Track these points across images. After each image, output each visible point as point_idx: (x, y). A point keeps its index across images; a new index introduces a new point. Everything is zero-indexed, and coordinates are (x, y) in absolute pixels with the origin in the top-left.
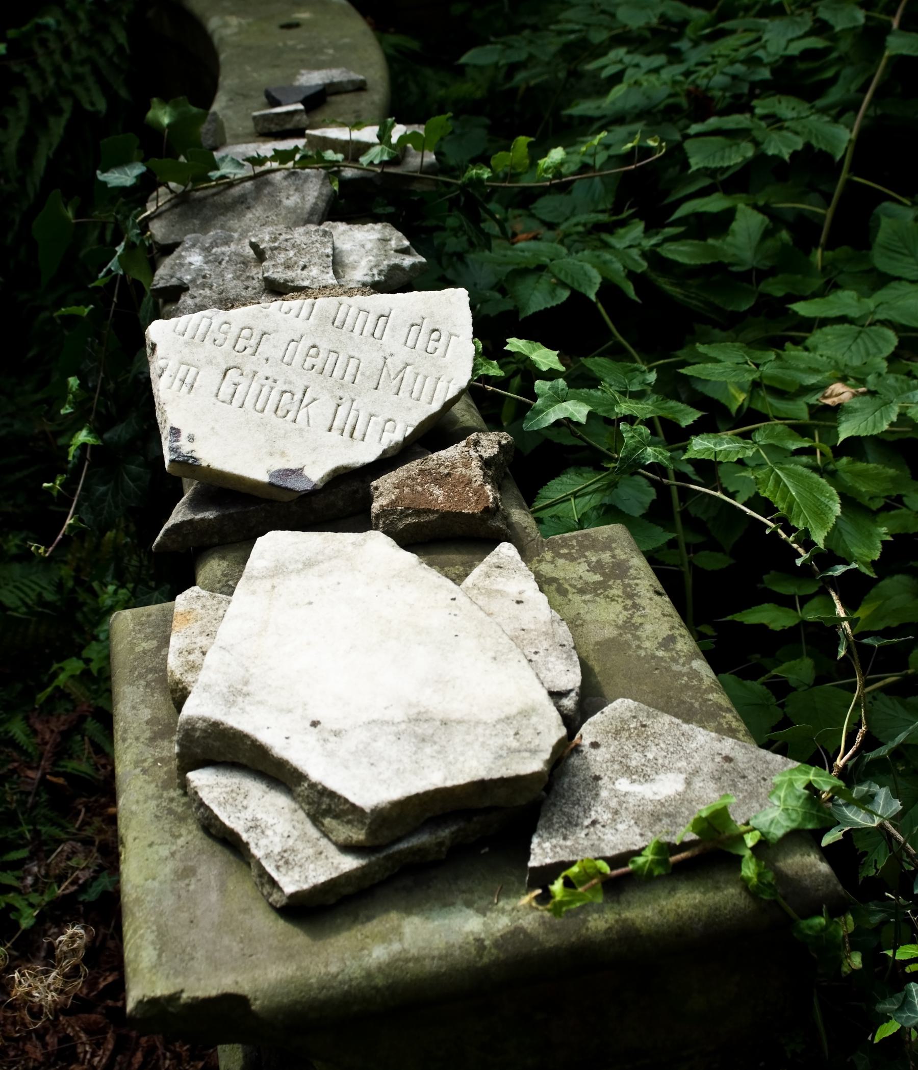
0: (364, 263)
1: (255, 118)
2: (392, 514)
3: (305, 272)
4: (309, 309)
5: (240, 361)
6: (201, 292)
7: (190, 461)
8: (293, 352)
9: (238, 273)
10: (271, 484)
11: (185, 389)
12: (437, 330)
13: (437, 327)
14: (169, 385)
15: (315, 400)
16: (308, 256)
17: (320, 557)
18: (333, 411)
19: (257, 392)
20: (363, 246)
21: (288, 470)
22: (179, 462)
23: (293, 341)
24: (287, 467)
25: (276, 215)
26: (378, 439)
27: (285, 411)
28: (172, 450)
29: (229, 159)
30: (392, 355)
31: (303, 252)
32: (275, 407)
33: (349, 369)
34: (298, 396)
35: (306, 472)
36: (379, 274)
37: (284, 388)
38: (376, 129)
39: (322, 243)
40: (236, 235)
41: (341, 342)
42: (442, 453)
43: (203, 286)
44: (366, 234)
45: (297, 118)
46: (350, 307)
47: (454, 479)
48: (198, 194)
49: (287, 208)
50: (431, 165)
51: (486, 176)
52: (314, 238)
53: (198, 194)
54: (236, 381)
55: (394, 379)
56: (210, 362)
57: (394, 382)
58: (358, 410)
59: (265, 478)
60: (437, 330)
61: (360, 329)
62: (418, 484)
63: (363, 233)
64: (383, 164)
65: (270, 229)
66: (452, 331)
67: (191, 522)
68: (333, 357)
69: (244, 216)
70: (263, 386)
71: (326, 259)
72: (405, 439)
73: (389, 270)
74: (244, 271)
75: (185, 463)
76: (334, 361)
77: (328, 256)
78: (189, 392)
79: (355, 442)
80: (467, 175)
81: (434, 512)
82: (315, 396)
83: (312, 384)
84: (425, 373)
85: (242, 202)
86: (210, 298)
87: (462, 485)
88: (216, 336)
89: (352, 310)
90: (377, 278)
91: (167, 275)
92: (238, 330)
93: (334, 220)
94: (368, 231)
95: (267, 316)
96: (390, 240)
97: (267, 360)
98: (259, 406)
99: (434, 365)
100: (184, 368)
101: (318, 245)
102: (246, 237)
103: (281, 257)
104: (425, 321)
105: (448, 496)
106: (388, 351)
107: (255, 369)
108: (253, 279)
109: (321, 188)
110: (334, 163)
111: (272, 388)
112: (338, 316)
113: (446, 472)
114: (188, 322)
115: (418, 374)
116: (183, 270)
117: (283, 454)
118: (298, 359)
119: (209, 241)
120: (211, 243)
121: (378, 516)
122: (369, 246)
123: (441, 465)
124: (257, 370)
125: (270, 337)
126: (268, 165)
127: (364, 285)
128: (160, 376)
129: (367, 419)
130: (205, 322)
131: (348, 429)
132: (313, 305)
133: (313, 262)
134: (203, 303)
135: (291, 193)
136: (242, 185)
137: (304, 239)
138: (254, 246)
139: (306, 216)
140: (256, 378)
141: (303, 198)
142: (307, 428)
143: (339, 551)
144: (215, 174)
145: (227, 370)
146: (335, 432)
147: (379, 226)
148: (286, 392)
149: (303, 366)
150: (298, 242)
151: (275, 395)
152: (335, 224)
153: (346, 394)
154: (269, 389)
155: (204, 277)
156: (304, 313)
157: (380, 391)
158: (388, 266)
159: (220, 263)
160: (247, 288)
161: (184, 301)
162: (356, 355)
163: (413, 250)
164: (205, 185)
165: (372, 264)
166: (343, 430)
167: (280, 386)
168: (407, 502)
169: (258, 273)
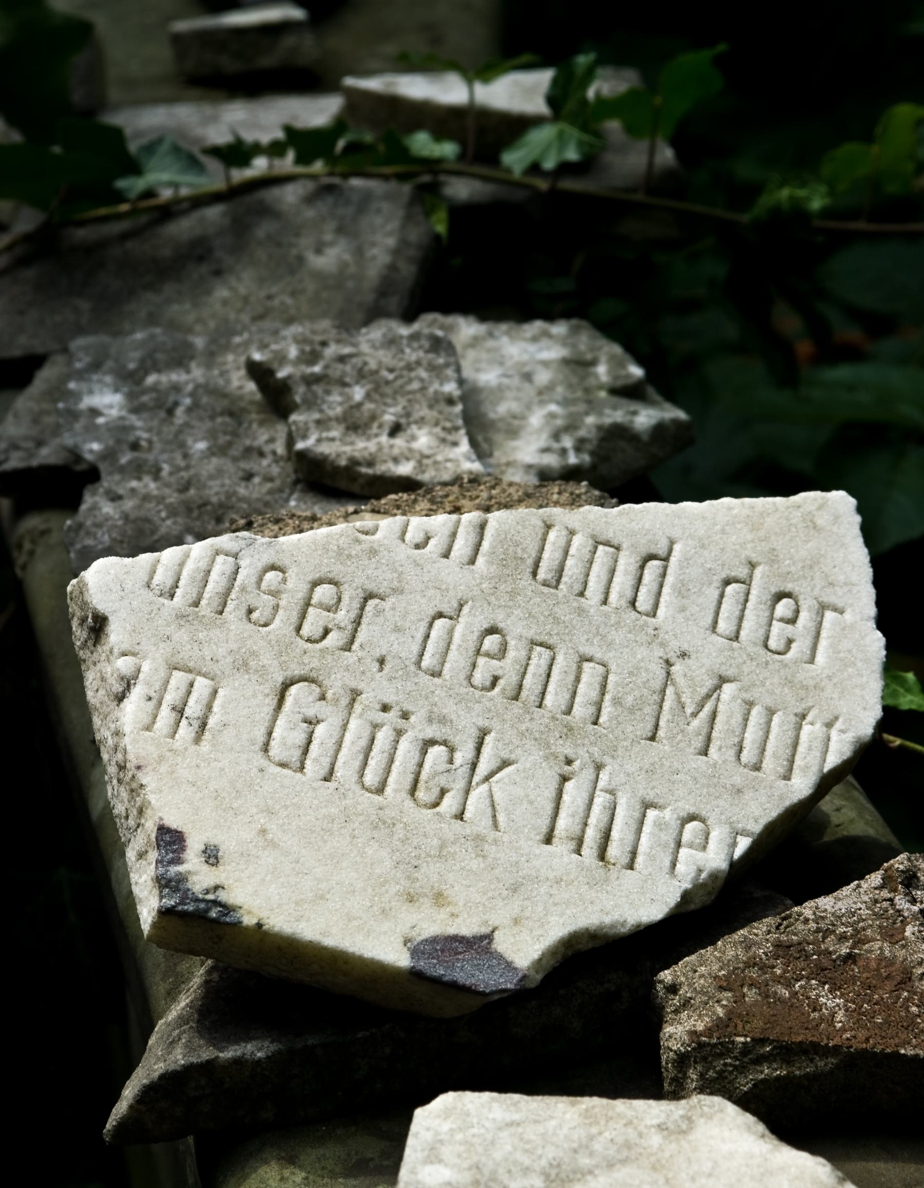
0: (536, 419)
1: (178, 40)
2: (721, 1055)
3: (399, 442)
4: (472, 538)
5: (315, 663)
6: (134, 484)
7: (213, 914)
8: (442, 644)
9: (223, 439)
10: (415, 974)
11: (185, 731)
12: (788, 595)
13: (789, 587)
14: (147, 720)
15: (505, 764)
16: (402, 402)
17: (585, 1161)
18: (551, 792)
19: (363, 742)
20: (528, 377)
21: (455, 938)
22: (184, 915)
23: (440, 615)
24: (452, 931)
25: (293, 294)
26: (667, 863)
27: (436, 792)
28: (164, 883)
29: (165, 147)
30: (684, 655)
31: (388, 390)
32: (410, 778)
33: (582, 688)
34: (463, 756)
35: (502, 944)
36: (578, 449)
37: (430, 732)
38: (544, 78)
39: (432, 368)
40: (199, 342)
41: (557, 621)
42: (825, 902)
43: (138, 470)
44: (532, 348)
45: (289, 41)
46: (572, 533)
47: (866, 968)
48: (81, 234)
49: (319, 276)
50: (669, 175)
51: (816, 205)
52: (411, 355)
53: (81, 234)
54: (311, 713)
55: (695, 715)
56: (242, 666)
57: (696, 723)
58: (612, 792)
59: (401, 959)
60: (788, 595)
61: (602, 589)
62: (778, 980)
63: (523, 345)
64: (565, 168)
65: (296, 329)
66: (825, 599)
67: (209, 1065)
68: (540, 657)
69: (208, 292)
70: (376, 726)
71: (448, 409)
72: (732, 864)
73: (602, 440)
74: (235, 434)
75: (199, 917)
76: (543, 670)
77: (450, 401)
78: (198, 739)
79: (614, 872)
80: (766, 201)
81: (826, 1051)
82: (505, 755)
83: (496, 725)
84: (769, 701)
85: (201, 259)
86: (160, 500)
87: (889, 985)
88: (252, 600)
89: (577, 541)
90: (572, 459)
91: (26, 438)
92: (305, 587)
93: (447, 310)
94: (535, 339)
95: (373, 552)
96: (593, 363)
97: (382, 661)
98: (371, 778)
99: (789, 682)
100: (179, 679)
101: (423, 374)
102: (227, 347)
103: (335, 404)
104: (758, 572)
105: (859, 1011)
106: (675, 645)
107: (353, 684)
108: (261, 454)
109: (403, 227)
110: (433, 165)
111: (399, 733)
112: (546, 555)
113: (844, 951)
114: (182, 565)
115: (750, 704)
116: (78, 426)
117: (439, 899)
118: (456, 660)
119: (136, 355)
120: (142, 361)
121: (682, 1060)
122: (543, 377)
123: (827, 933)
124: (361, 686)
125: (387, 604)
126: (260, 165)
127: (545, 476)
128: (120, 698)
129: (637, 815)
130: (222, 565)
131: (592, 835)
132: (482, 526)
133: (416, 415)
134: (142, 513)
135: (328, 237)
136: (196, 215)
137: (385, 356)
138: (258, 372)
139: (370, 298)
140: (358, 708)
141: (359, 252)
142: (493, 834)
143: (628, 1145)
144: (133, 185)
145: (286, 686)
146: (561, 848)
147: (559, 329)
148: (432, 742)
149: (469, 677)
150: (373, 365)
151: (406, 748)
152: (450, 320)
153: (582, 752)
154: (391, 735)
155: (135, 446)
156: (461, 547)
157: (663, 746)
158: (600, 428)
159: (170, 412)
160: (248, 477)
161: (94, 508)
162: (598, 655)
163: (651, 391)
164: (103, 211)
165: (559, 422)
166: (580, 842)
167: (419, 729)
168: (758, 1024)
169: (272, 440)
